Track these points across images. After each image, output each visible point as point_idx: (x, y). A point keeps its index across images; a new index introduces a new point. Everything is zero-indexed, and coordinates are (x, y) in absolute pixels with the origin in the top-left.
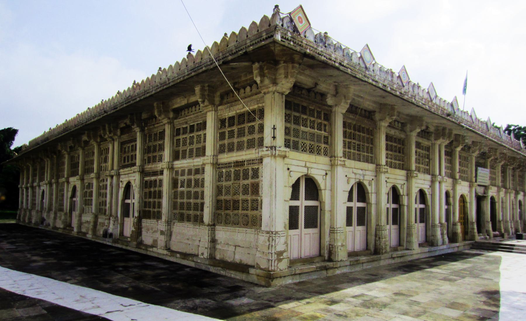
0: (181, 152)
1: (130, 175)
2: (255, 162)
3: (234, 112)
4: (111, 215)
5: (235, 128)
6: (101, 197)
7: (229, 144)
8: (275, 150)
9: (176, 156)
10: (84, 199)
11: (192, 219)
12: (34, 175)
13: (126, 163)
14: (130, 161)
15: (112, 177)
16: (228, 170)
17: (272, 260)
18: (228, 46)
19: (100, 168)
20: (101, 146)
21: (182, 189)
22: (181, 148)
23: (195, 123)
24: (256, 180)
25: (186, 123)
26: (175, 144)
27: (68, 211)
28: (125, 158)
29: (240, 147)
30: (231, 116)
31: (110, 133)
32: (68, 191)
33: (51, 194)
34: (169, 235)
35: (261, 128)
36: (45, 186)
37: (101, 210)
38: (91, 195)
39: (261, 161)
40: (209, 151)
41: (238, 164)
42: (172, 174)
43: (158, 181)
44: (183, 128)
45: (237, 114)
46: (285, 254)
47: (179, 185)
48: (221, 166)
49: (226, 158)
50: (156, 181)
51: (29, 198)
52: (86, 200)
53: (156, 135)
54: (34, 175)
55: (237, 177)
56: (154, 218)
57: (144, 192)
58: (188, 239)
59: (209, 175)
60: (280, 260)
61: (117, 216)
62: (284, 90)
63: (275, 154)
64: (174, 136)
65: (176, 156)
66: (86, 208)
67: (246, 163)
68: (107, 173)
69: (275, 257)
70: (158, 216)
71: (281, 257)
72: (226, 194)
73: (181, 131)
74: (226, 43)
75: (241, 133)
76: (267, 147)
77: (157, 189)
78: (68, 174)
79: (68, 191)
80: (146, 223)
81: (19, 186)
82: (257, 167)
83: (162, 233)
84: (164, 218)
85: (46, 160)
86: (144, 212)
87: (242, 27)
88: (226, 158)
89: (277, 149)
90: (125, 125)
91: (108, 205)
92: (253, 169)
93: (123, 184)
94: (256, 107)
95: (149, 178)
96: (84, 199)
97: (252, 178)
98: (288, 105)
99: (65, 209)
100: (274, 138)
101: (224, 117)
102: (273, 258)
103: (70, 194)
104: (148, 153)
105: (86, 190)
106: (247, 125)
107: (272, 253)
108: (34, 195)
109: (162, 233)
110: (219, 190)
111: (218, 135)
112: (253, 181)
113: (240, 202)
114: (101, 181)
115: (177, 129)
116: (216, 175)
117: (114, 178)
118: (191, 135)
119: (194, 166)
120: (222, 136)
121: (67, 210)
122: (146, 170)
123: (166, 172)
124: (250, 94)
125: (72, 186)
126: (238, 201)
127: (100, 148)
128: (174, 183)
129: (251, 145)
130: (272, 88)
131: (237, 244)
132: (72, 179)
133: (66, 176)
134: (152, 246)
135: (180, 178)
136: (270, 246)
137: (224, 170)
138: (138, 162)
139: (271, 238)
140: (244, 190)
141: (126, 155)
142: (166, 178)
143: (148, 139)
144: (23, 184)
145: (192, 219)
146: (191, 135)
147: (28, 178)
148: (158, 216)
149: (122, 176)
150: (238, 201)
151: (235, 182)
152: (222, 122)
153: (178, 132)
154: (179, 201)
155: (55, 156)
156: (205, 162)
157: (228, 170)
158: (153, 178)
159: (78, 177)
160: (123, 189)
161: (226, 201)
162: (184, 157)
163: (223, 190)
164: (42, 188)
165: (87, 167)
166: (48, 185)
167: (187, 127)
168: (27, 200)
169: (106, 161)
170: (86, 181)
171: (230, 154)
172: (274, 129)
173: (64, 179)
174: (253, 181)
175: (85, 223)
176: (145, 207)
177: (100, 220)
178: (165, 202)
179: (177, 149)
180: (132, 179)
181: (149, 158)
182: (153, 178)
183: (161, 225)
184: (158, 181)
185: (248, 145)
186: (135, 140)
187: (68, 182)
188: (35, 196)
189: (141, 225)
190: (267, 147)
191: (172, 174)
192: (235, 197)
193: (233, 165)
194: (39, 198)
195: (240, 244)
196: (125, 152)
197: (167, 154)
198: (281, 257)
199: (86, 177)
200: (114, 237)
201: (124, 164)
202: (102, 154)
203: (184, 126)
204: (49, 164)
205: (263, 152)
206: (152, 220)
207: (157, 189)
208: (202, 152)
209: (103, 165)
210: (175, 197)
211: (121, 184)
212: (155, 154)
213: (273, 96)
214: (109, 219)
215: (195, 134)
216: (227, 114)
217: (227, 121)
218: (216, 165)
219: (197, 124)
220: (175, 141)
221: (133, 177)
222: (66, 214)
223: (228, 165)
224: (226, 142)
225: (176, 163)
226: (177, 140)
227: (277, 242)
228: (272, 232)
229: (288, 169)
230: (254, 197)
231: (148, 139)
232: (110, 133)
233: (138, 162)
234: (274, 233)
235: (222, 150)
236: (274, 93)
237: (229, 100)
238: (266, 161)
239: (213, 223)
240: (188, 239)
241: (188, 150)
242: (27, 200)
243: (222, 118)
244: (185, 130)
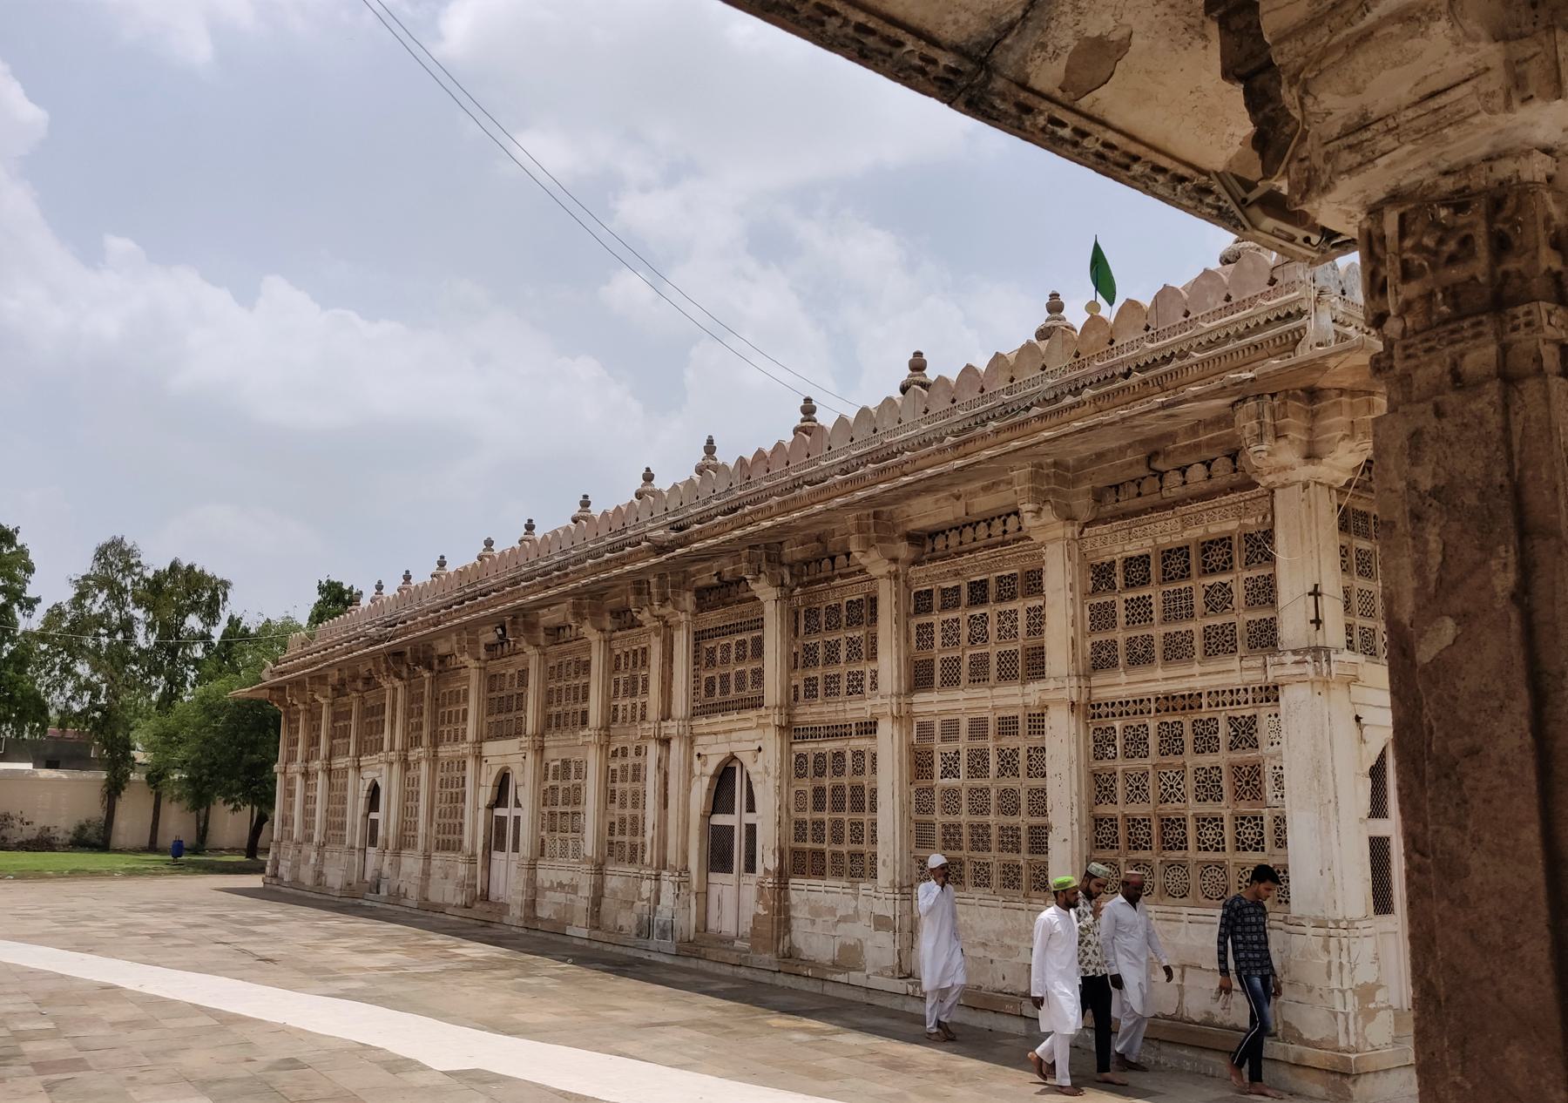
0: (938, 665)
1: (734, 736)
2: (1242, 696)
3: (1149, 542)
4: (663, 864)
5: (1154, 593)
6: (615, 808)
7: (1130, 642)
8: (1328, 660)
9: (920, 677)
10: (546, 810)
11: (996, 879)
12: (339, 733)
13: (717, 697)
14: (733, 691)
15: (665, 742)
16: (1134, 722)
17: (1346, 1016)
18: (1112, 342)
19: (612, 716)
20: (615, 644)
21: (950, 782)
22: (938, 654)
23: (992, 577)
24: (1250, 755)
25: (957, 574)
26: (914, 638)
27: (479, 851)
28: (711, 681)
29: (1177, 650)
30: (1135, 553)
31: (662, 604)
32: (478, 785)
33: (409, 797)
34: (906, 929)
35: (1265, 592)
36: (385, 767)
37: (621, 844)
38: (575, 796)
39: (1271, 693)
40: (1058, 659)
41: (1169, 703)
42: (909, 733)
43: (849, 755)
44: (944, 591)
45: (1156, 547)
46: (1380, 996)
47: (938, 769)
48: (1104, 710)
49: (1120, 685)
50: (839, 755)
51: (319, 808)
52: (552, 814)
53: (836, 609)
54: (339, 733)
55: (1171, 742)
56: (839, 874)
57: (793, 791)
58: (984, 945)
59: (1064, 743)
60: (1369, 1015)
61: (686, 870)
62: (1337, 474)
63: (1330, 673)
64: (908, 615)
65: (920, 677)
66: (554, 841)
67: (1204, 701)
68: (649, 727)
69: (1352, 1002)
70: (860, 867)
71: (1372, 1006)
72: (1129, 800)
73: (937, 600)
74: (1104, 334)
75: (1178, 609)
76: (1295, 652)
77: (845, 780)
78: (479, 731)
79: (478, 785)
80: (805, 893)
81: (276, 768)
82: (1247, 713)
83: (881, 923)
84: (884, 875)
85: (386, 685)
86: (797, 853)
87: (226, 584)
88: (1120, 685)
89: (1333, 657)
90: (715, 580)
91: (649, 833)
92: (1232, 720)
93: (705, 764)
94: (1232, 525)
95: (814, 745)
96: (546, 810)
97: (1233, 747)
98: (1349, 522)
99: (467, 843)
100: (1317, 622)
101: (1107, 559)
102: (1349, 1009)
103: (486, 795)
104: (805, 666)
105: (551, 782)
106: (1199, 585)
107: (1343, 992)
108: (337, 799)
109: (881, 923)
110: (1101, 786)
111: (1087, 613)
112: (1239, 756)
113: (1191, 825)
114: (615, 754)
115: (918, 594)
116: (1086, 738)
117: (674, 744)
118: (978, 612)
119: (995, 708)
120: (1102, 618)
121: (474, 844)
122: (798, 719)
123: (885, 728)
124: (1205, 486)
125: (496, 770)
126: (1181, 822)
127: (611, 650)
128: (920, 763)
129: (1219, 643)
130: (1304, 472)
131: (1188, 962)
132: (490, 748)
133: (471, 736)
134: (837, 966)
135: (939, 747)
136: (1334, 969)
137: (1117, 724)
138: (773, 689)
139: (1333, 942)
140: (1201, 784)
141: (714, 672)
142: (889, 746)
143: (802, 623)
144: (291, 758)
145: (996, 879)
146: (978, 612)
147: (314, 742)
148: (860, 867)
149: (700, 740)
150: (1181, 822)
151: (1166, 760)
152: (1102, 575)
153: (923, 602)
154: (939, 818)
155: (427, 675)
156: (1046, 697)
157: (1134, 722)
158: (829, 746)
159: (525, 741)
160: (706, 780)
161: (1133, 822)
162: (951, 681)
163: (1119, 785)
164: (368, 775)
165: (554, 709)
166: (396, 767)
167: (957, 589)
168: (308, 813)
169: (635, 687)
170: (550, 754)
171: (1139, 674)
172: (1316, 593)
173: (465, 748)
174: (1239, 756)
175: (551, 888)
176: (800, 837)
177: (613, 883)
178: (889, 819)
179: (923, 656)
180: (742, 746)
181: (811, 683)
182: (829, 746)
183: (877, 897)
184: (849, 755)
185: (1207, 645)
186: (758, 624)
187: (479, 757)
188: (343, 800)
189: (787, 898)
190: (1295, 652)
191: (909, 733)
192: (1169, 808)
193: (1153, 706)
194: (355, 807)
195: (1198, 962)
196: (711, 662)
197: (888, 666)
198: (1372, 1006)
199: (550, 741)
200: (677, 935)
201: (710, 701)
202: (617, 668)
203: (950, 584)
204: (400, 697)
205: (1282, 668)
206: (829, 882)
207: (845, 780)
208: (1035, 664)
209: (623, 702)
210: (924, 806)
211: (697, 763)
212: (832, 671)
213: (1303, 495)
214: (657, 878)
215: (991, 610)
216: (1117, 549)
217: (1118, 569)
218: (1089, 710)
219: (1000, 579)
220: (914, 631)
221: (757, 746)
222: (472, 859)
223: (1124, 707)
224: (1120, 635)
225: (919, 698)
226: (919, 627)
227: (1354, 956)
228: (1337, 922)
229: (1358, 719)
230: (1244, 808)
231: (802, 623)
232: (662, 604)
233: (773, 689)
234: (1343, 924)
235: (1102, 660)
236: (1306, 486)
237: (1122, 504)
238: (1288, 696)
239: (492, 898)
240: (984, 945)
241: (967, 660)
242: (308, 813)
243: (1098, 562)
244: (951, 599)
